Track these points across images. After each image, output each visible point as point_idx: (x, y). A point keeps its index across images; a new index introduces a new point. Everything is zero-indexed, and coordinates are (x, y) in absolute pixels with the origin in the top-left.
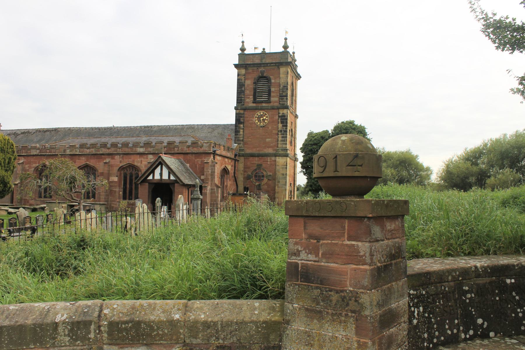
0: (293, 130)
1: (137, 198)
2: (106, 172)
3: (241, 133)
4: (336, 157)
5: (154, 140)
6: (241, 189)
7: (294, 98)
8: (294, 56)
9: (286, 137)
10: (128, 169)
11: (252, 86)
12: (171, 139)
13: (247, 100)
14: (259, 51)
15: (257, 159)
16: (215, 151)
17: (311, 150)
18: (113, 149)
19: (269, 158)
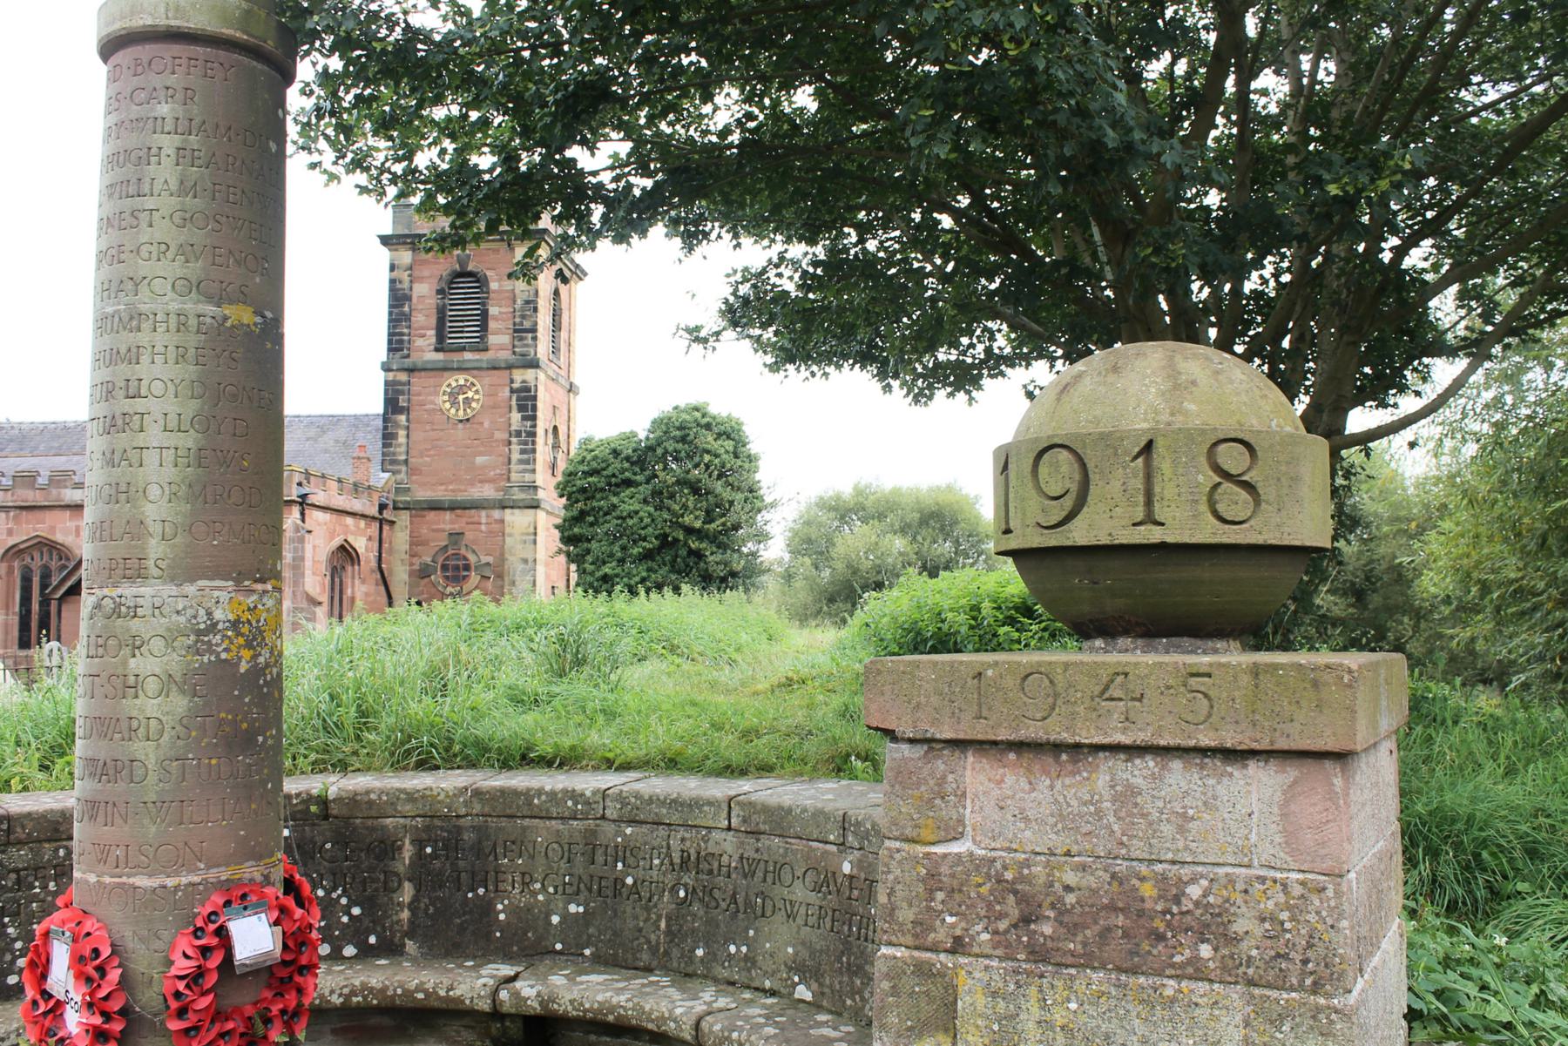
0: (562, 430)
3: (402, 439)
4: (1149, 447)
7: (564, 334)
9: (534, 451)
10: (37, 555)
11: (432, 301)
13: (419, 342)
15: (448, 515)
17: (583, 490)
19: (483, 513)
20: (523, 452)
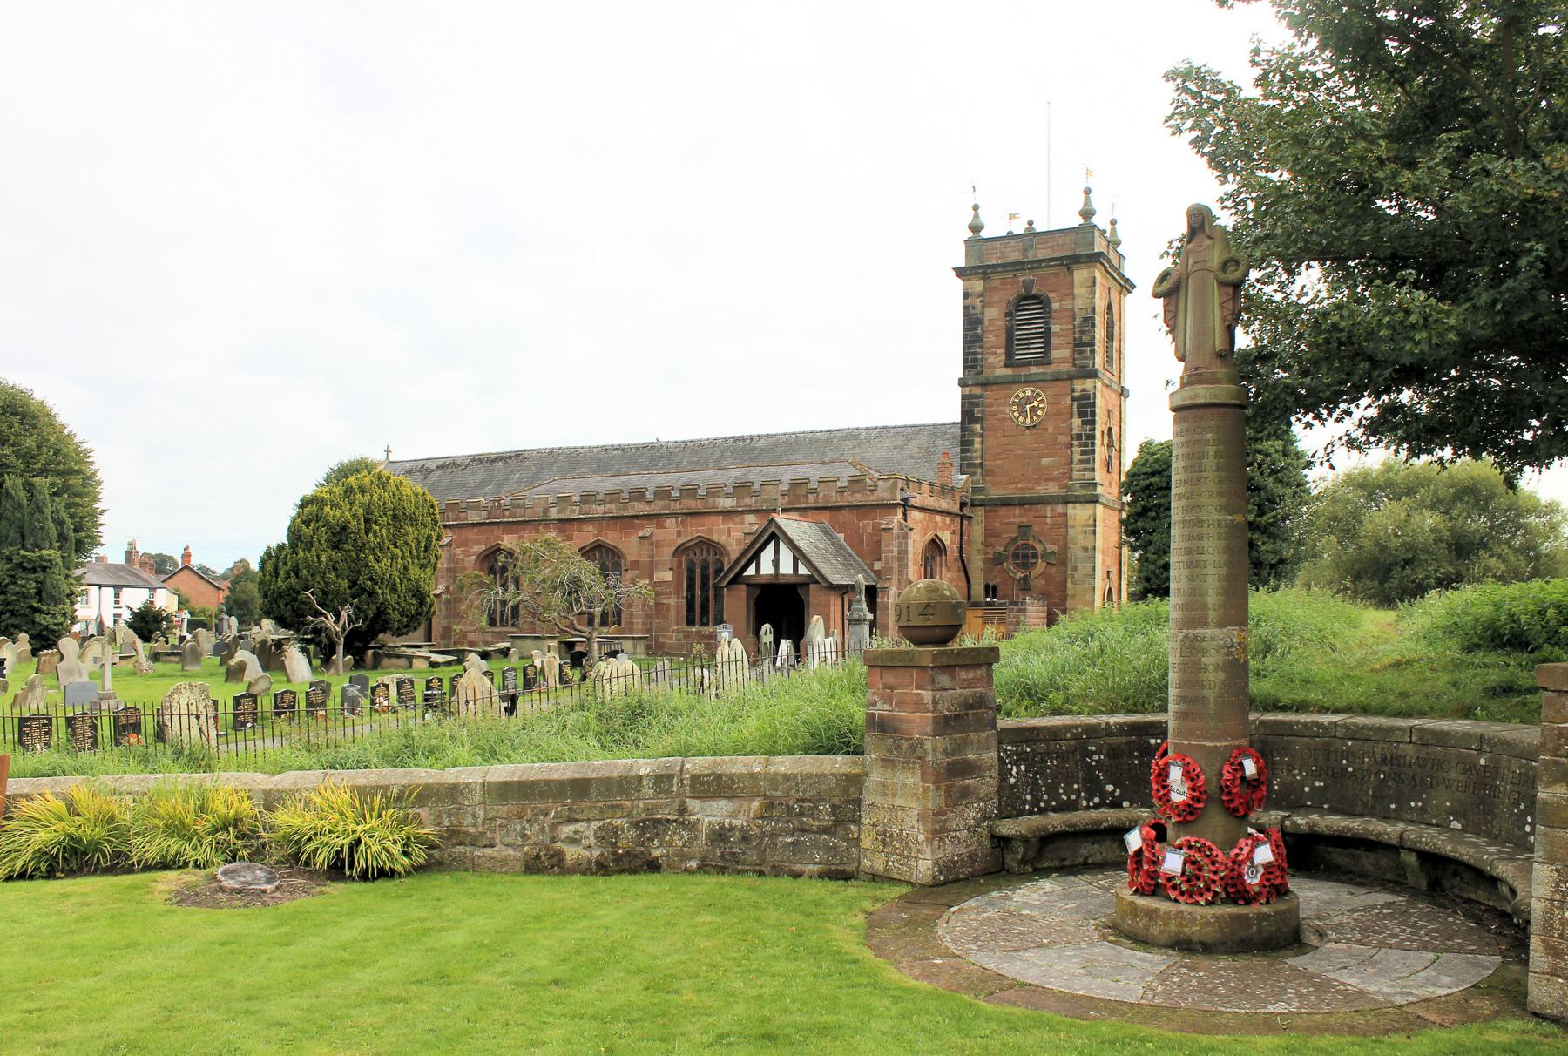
0: (1115, 430)
1: (720, 621)
2: (644, 559)
3: (977, 446)
5: (757, 475)
6: (978, 590)
7: (1116, 344)
8: (1114, 231)
9: (1093, 452)
10: (698, 552)
11: (1001, 323)
12: (800, 472)
13: (991, 360)
14: (1019, 228)
15: (1017, 511)
16: (906, 500)
18: (660, 503)
19: (1048, 508)
20: (1083, 453)
